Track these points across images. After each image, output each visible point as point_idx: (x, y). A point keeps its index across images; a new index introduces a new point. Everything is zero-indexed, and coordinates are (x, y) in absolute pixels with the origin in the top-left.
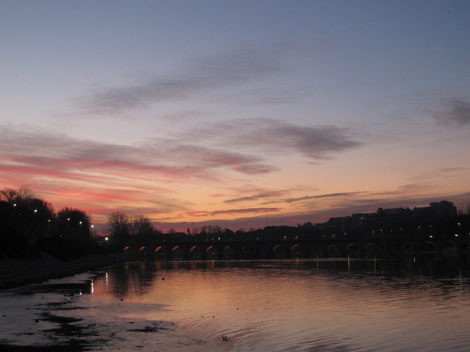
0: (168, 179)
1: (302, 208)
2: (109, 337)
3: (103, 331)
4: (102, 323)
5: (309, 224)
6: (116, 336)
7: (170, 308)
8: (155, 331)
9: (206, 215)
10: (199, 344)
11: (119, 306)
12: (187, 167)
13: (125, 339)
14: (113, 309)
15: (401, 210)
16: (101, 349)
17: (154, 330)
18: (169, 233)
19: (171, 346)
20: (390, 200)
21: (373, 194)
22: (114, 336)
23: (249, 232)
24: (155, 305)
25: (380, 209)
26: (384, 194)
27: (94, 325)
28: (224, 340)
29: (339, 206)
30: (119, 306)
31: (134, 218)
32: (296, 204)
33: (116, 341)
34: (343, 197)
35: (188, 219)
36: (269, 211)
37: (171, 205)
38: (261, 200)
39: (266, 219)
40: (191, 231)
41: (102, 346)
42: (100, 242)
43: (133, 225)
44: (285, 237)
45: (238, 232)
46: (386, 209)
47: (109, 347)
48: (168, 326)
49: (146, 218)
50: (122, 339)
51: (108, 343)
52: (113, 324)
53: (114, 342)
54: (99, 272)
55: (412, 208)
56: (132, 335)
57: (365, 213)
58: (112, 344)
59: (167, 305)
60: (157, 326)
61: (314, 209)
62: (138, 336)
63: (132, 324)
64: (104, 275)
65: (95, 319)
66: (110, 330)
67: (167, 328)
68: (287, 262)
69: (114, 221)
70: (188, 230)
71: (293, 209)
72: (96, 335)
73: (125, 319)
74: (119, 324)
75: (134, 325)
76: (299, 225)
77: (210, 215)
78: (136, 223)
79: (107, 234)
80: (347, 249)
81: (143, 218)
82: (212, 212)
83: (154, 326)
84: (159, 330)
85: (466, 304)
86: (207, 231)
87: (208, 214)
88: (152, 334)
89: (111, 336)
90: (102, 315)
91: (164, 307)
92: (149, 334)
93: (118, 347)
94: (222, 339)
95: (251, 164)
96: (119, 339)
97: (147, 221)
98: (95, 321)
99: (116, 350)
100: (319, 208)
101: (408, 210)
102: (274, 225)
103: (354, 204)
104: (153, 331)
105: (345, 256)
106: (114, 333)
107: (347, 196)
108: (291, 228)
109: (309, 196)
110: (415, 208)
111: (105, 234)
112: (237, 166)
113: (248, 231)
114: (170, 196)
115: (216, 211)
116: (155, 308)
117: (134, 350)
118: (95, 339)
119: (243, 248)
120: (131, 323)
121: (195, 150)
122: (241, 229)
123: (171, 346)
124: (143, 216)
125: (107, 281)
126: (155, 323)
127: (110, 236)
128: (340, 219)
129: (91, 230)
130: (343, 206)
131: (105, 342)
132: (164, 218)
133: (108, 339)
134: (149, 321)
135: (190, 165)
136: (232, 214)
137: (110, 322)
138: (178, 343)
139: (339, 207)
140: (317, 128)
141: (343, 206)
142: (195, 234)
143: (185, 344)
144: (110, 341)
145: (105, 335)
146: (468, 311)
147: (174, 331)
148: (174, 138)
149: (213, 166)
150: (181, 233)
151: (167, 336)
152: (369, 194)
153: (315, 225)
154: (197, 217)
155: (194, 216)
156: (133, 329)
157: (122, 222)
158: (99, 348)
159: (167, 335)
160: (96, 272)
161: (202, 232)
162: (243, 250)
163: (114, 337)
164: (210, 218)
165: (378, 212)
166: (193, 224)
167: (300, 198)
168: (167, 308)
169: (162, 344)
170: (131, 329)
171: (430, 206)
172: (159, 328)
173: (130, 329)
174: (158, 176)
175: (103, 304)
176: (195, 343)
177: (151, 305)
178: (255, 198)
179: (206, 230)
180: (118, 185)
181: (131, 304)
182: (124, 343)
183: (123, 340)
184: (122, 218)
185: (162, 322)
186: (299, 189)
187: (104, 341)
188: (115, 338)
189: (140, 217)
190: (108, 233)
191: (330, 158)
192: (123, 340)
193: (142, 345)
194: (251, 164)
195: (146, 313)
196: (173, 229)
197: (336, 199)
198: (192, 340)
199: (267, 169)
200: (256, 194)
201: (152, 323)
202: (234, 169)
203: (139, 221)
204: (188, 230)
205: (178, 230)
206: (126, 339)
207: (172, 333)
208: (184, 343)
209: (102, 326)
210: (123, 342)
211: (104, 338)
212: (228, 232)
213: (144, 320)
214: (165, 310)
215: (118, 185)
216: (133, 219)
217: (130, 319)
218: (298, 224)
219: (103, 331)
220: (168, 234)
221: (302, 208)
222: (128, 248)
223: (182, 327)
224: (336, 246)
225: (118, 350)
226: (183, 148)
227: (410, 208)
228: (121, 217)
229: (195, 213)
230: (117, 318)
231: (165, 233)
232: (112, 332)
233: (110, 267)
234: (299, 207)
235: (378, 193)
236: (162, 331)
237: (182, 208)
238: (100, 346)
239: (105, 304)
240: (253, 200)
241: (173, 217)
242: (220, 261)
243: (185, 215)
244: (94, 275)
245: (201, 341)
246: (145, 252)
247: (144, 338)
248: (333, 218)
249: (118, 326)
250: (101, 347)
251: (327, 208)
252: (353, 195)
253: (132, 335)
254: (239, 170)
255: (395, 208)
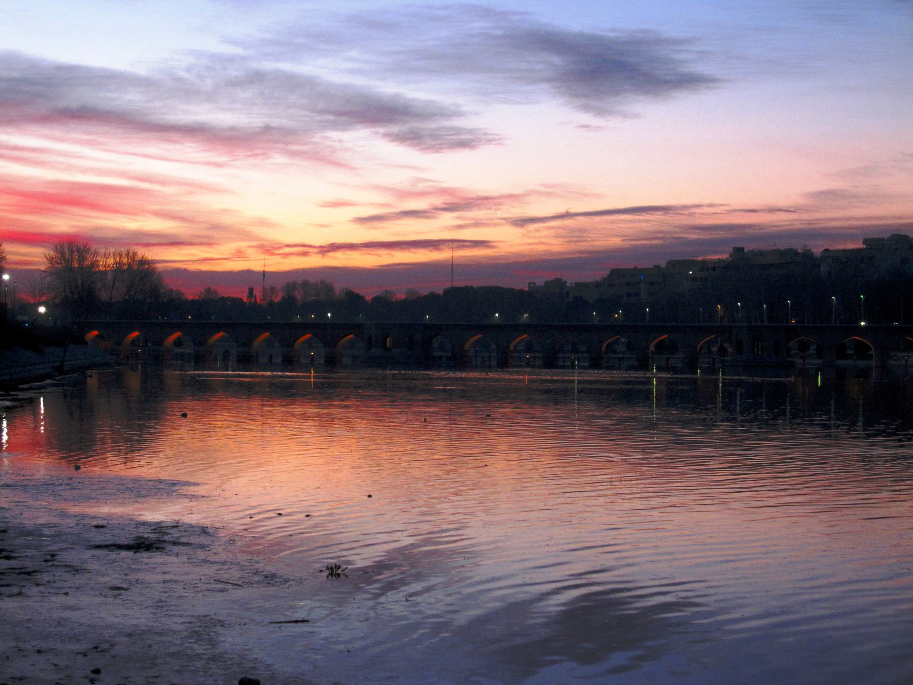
0: (212, 157)
1: (553, 241)
2: (43, 563)
3: (27, 547)
4: (24, 528)
5: (559, 283)
6: (59, 561)
7: (200, 490)
8: (158, 548)
9: (305, 254)
10: (268, 583)
11: (68, 484)
12: (267, 129)
13: (81, 570)
14: (54, 491)
15: (793, 252)
16: (20, 594)
17: (155, 545)
18: (201, 299)
19: (198, 587)
20: (778, 229)
21: (735, 210)
22: (54, 560)
23: (405, 300)
24: (160, 481)
25: (739, 250)
26: (763, 211)
27: (5, 531)
28: (331, 574)
29: (647, 239)
30: (68, 484)
31: (114, 259)
32: (537, 230)
33: (58, 574)
34: (658, 216)
35: (257, 263)
36: (467, 247)
37: (217, 227)
38: (448, 219)
39: (451, 267)
40: (258, 293)
41: (24, 586)
42: (26, 318)
43: (110, 276)
44: (497, 315)
45: (378, 300)
46: (753, 251)
47: (41, 588)
48: (191, 537)
49: (144, 259)
50: (76, 570)
51: (38, 576)
52: (53, 529)
53: (54, 576)
54: (22, 395)
55: (817, 251)
56: (98, 558)
57: (700, 259)
58: (49, 582)
59: (191, 483)
60: (163, 535)
61: (581, 244)
62: (114, 561)
63: (101, 530)
64: (33, 402)
65: (7, 515)
66: (46, 545)
67: (190, 542)
68: (263, 376)
69: (62, 264)
70: (251, 290)
71: (530, 244)
72: (8, 558)
73: (83, 516)
74: (67, 530)
75: (106, 533)
76: (533, 285)
77: (316, 253)
78: (119, 270)
79: (44, 298)
80: (652, 348)
81: (137, 259)
82: (321, 247)
83: (156, 535)
84: (169, 547)
85: (809, 489)
86: (299, 296)
87: (310, 250)
88: (150, 558)
89: (46, 561)
90: (26, 506)
91: (184, 488)
92: (144, 556)
93: (62, 588)
94: (328, 572)
95: (432, 125)
96: (68, 569)
97: (146, 266)
98: (7, 522)
99: (59, 596)
100: (596, 243)
101: (808, 255)
102: (469, 284)
103: (684, 236)
104: (154, 550)
105: (644, 365)
106: (54, 553)
107: (668, 213)
108: (511, 291)
109: (573, 210)
110: (827, 250)
111: (38, 298)
112: (395, 129)
113: (403, 296)
114: (213, 203)
115: (333, 244)
116: (160, 489)
117: (105, 596)
118: (6, 569)
119: (388, 339)
120: (97, 527)
121: (292, 83)
122: (386, 291)
123: (198, 587)
124: (135, 254)
125: (5, 418)
126: (158, 527)
127: (51, 302)
128: (635, 272)
129: (4, 285)
130: (658, 238)
131: (31, 575)
132: (197, 258)
133: (37, 569)
134: (144, 524)
135: (275, 122)
136: (372, 252)
137: (45, 524)
138: (215, 580)
139: (646, 242)
140: (612, 35)
141: (658, 238)
142: (267, 302)
143: (235, 582)
144: (44, 574)
145: (31, 558)
146: (293, 496)
147: (207, 549)
148: (238, 51)
149: (334, 126)
150: (232, 298)
151: (189, 563)
152: (725, 210)
153: (573, 285)
154: (282, 258)
155: (273, 254)
156: (102, 543)
157: (82, 268)
158: (15, 590)
159: (188, 558)
160: (13, 395)
161: (286, 297)
162: (388, 345)
163: (55, 563)
164: (314, 261)
165: (731, 259)
166: (264, 277)
167: (549, 216)
168: (192, 490)
169: (176, 582)
170: (98, 543)
171: (864, 246)
172: (169, 542)
173: (95, 543)
174: (190, 149)
175: (31, 478)
176: (258, 582)
177: (150, 483)
178: (432, 213)
179: (296, 292)
180: (85, 171)
181: (101, 480)
182: (79, 580)
183: (77, 571)
184: (82, 258)
185: (177, 527)
186: (548, 192)
187: (29, 573)
188: (56, 566)
189: (127, 254)
190: (46, 296)
191: (636, 116)
192: (77, 571)
193: (124, 586)
194: (432, 125)
195: (136, 502)
196: (254, 290)
197: (640, 221)
198: (250, 575)
199: (470, 137)
200: (438, 201)
201: (152, 528)
202: (386, 135)
203: (125, 264)
204: (251, 290)
205: (225, 292)
206: (85, 569)
207: (201, 555)
208: (231, 582)
209: (23, 532)
210: (78, 576)
211: (29, 565)
212: (353, 299)
213: (132, 520)
214: (186, 496)
215: (85, 171)
216: (111, 261)
217: (95, 517)
218: (529, 283)
219: (27, 547)
220: (198, 300)
221: (553, 241)
222: (98, 336)
223: (227, 539)
224: (623, 340)
225: (63, 595)
226: (258, 78)
227: (814, 250)
228: (238, 252)
229: (279, 248)
230: (64, 514)
231: (191, 297)
232: (49, 551)
233: (48, 381)
234: (544, 240)
235: (746, 208)
236: (176, 549)
237: (244, 235)
238: (19, 586)
239: (34, 477)
240: (427, 218)
241: (221, 256)
242: (284, 372)
243: (251, 252)
244: (8, 403)
245: (274, 576)
246: (141, 344)
247: (131, 568)
248: (618, 270)
249: (65, 534)
250: (21, 590)
251: (615, 242)
252: (686, 212)
253: (98, 558)
254: (400, 138)
255: (776, 248)
